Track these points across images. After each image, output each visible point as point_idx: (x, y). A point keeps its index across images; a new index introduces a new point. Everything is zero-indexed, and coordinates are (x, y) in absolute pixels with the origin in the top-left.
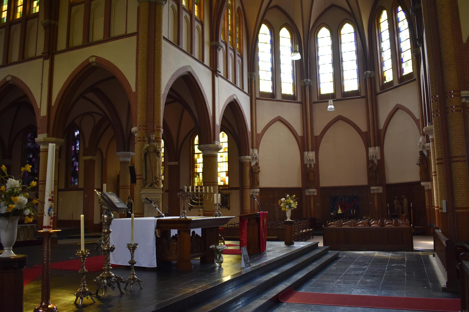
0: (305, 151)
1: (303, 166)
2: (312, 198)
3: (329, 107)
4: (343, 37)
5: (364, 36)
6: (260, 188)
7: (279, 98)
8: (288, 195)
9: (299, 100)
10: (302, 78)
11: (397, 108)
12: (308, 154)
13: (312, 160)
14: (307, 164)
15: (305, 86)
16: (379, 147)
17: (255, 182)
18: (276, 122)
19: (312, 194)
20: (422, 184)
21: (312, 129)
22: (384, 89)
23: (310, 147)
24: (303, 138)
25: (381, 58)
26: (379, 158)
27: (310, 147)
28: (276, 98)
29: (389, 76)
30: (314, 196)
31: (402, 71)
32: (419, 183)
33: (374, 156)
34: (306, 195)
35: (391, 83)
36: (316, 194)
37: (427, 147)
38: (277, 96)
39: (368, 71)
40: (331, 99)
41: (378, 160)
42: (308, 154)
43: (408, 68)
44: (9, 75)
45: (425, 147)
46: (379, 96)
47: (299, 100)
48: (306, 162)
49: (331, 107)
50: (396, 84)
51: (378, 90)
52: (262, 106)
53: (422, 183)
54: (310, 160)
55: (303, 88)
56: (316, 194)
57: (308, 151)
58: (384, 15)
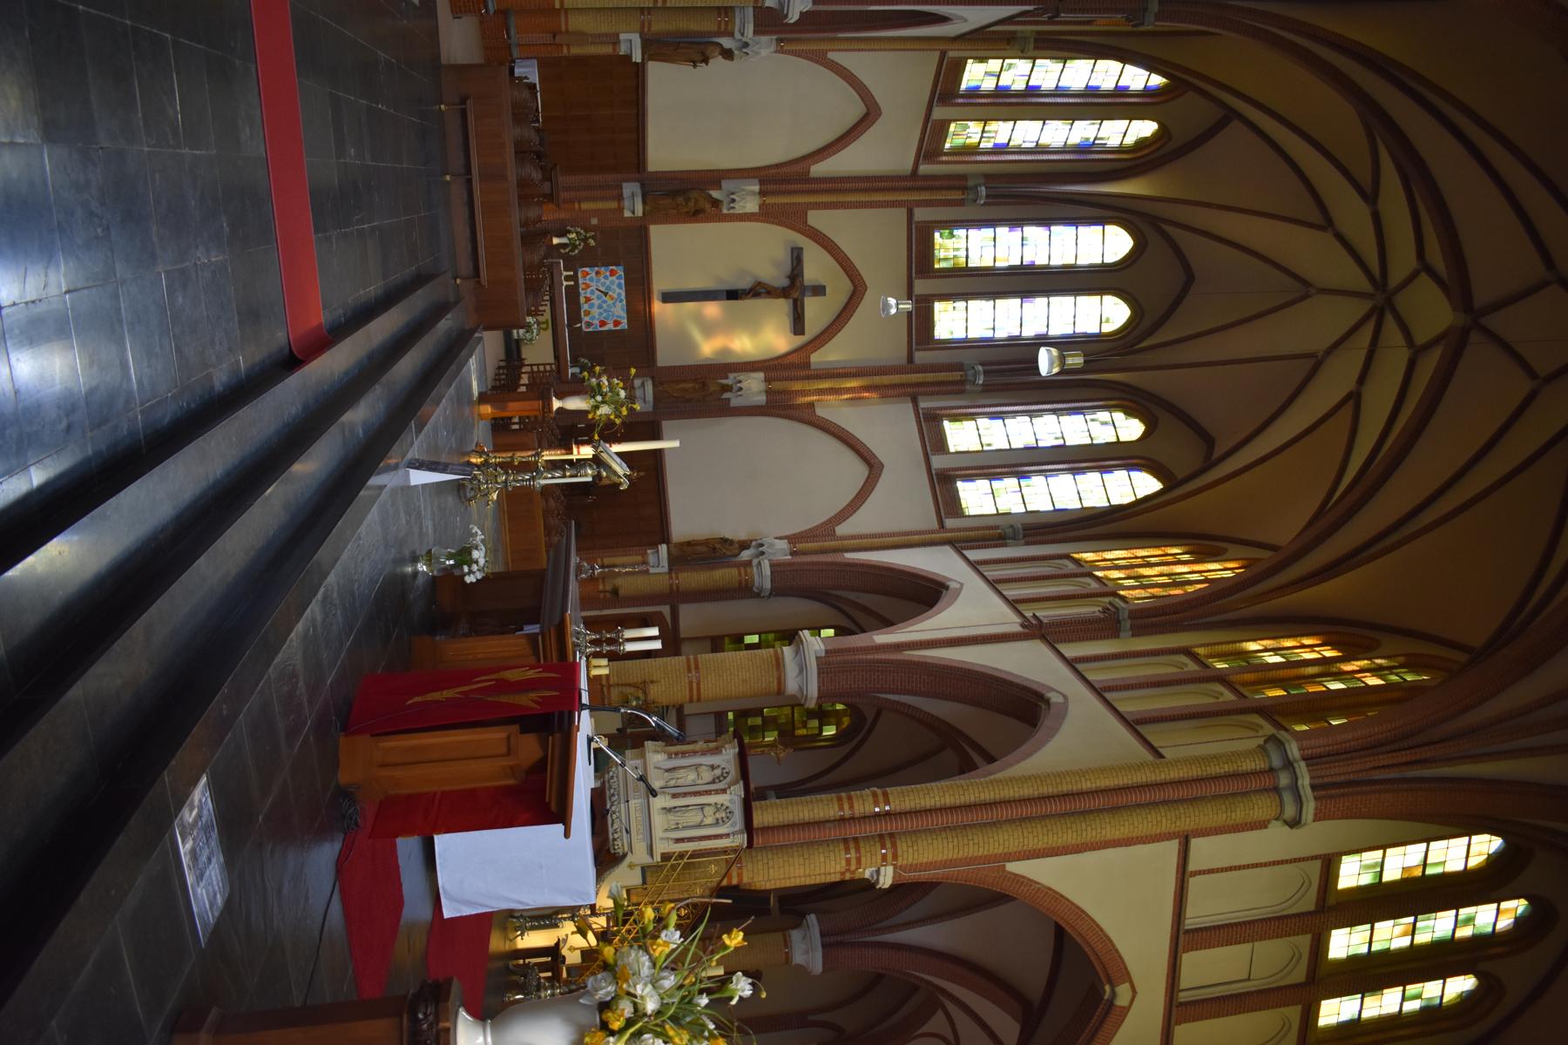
0: (761, 185)
1: (715, 178)
2: (613, 205)
3: (892, 301)
4: (1094, 300)
5: (1091, 194)
6: (643, 64)
7: (939, 113)
8: (633, 371)
9: (924, 169)
10: (989, 178)
11: (874, 467)
12: (753, 193)
13: (733, 208)
14: (720, 188)
15: (964, 189)
16: (764, 403)
17: (661, 47)
18: (862, 104)
19: (627, 203)
20: (663, 548)
21: (833, 50)
22: (925, 421)
23: (777, 385)
24: (805, 178)
25: (1015, 414)
26: (735, 402)
27: (770, 200)
28: (937, 106)
29: (962, 436)
30: (621, 210)
31: (969, 478)
32: (665, 538)
33: (732, 205)
34: (625, 185)
35: (940, 444)
36: (627, 214)
37: (759, 563)
38: (941, 108)
39: (982, 377)
40: (916, 308)
41: (729, 400)
42: (753, 193)
43: (976, 498)
44: (1065, 697)
45: (761, 557)
46: (908, 407)
47: (921, 357)
48: (725, 184)
49: (891, 307)
50: (938, 462)
51: (924, 404)
52: (918, 72)
53: (664, 547)
54: (733, 201)
55: (958, 183)
56: (627, 214)
57: (762, 193)
58: (1131, 429)
